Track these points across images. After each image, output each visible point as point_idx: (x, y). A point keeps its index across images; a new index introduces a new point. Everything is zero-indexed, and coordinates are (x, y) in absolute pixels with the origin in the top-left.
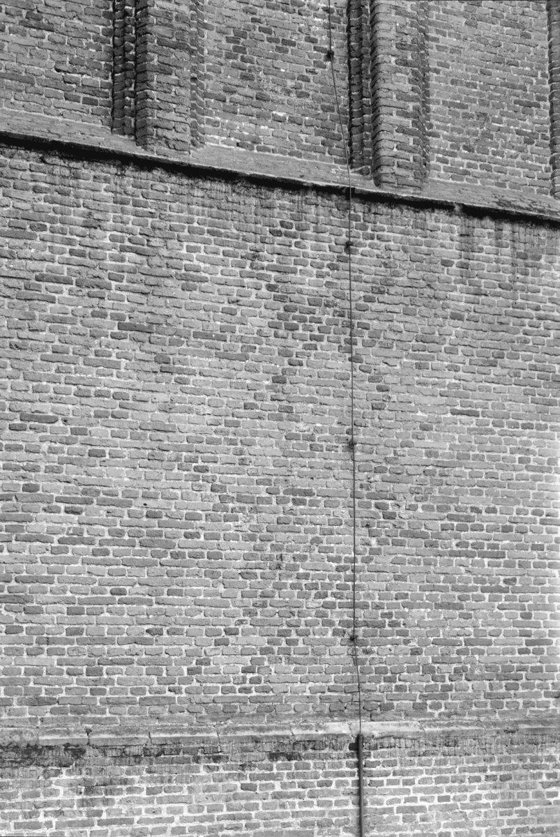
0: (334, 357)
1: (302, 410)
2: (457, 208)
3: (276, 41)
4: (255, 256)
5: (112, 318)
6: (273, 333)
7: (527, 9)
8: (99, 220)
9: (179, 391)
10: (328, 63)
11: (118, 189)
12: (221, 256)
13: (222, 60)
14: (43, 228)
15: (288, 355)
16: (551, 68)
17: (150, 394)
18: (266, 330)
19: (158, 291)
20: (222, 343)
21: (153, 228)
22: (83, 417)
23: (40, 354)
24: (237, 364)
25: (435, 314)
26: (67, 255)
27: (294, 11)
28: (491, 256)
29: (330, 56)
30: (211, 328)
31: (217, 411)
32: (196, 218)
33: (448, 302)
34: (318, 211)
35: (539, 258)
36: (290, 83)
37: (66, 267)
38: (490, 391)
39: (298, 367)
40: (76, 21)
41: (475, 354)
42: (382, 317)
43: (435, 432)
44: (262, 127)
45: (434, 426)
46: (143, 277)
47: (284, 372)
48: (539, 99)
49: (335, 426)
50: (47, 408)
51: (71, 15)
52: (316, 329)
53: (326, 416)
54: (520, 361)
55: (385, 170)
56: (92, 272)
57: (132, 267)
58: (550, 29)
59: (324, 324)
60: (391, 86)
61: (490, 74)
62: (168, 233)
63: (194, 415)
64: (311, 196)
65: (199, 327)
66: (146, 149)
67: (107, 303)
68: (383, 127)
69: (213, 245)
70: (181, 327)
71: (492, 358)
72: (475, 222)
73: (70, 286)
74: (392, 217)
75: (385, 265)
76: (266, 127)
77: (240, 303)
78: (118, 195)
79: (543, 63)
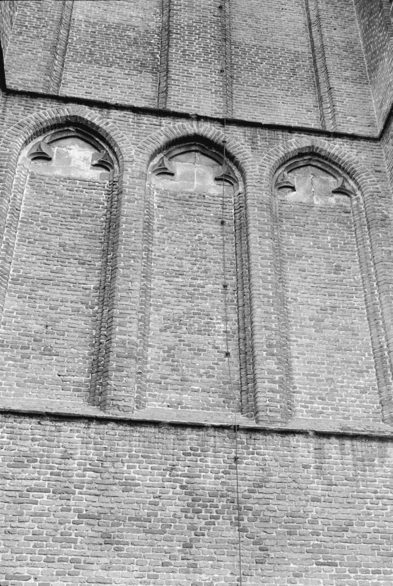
0: (227, 529)
1: (203, 565)
2: (311, 433)
3: (194, 350)
4: (173, 468)
5: (74, 511)
6: (184, 515)
7: (355, 321)
8: (71, 454)
9: (116, 556)
10: (227, 359)
11: (85, 436)
12: (150, 470)
13: (160, 362)
14: (36, 461)
15: (195, 529)
16: (373, 350)
17: (96, 558)
18: (179, 514)
19: (106, 493)
20: (148, 523)
21: (106, 456)
22: (48, 575)
23: (24, 536)
24: (158, 536)
25: (300, 499)
26: (49, 476)
27: (205, 334)
28: (338, 461)
29: (227, 354)
30: (140, 514)
31: (142, 568)
32: (134, 449)
33: (308, 490)
34: (214, 440)
35: (374, 460)
36: (202, 371)
37: (47, 482)
38: (345, 548)
39: (201, 537)
40: (72, 350)
41: (331, 524)
42: (261, 502)
43: (305, 578)
44: (184, 396)
45: (304, 574)
46: (97, 485)
47: (191, 540)
48: (368, 368)
49: (228, 575)
50: (24, 571)
51: (70, 347)
52: (215, 511)
53: (222, 569)
54: (366, 527)
55: (261, 414)
56: (63, 484)
57: (90, 480)
58: (370, 330)
59: (220, 508)
60: (263, 367)
61: (333, 357)
62: (115, 459)
63: (126, 571)
64: (211, 432)
65: (133, 514)
66: (105, 412)
67: (72, 502)
68: (258, 390)
69: (144, 464)
70: (120, 514)
71: (344, 526)
72: (325, 440)
73: (48, 494)
74: (266, 441)
75: (263, 469)
76: (187, 395)
77: (161, 498)
78: (85, 439)
79: (369, 348)
